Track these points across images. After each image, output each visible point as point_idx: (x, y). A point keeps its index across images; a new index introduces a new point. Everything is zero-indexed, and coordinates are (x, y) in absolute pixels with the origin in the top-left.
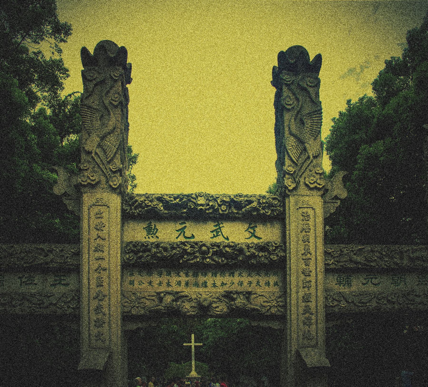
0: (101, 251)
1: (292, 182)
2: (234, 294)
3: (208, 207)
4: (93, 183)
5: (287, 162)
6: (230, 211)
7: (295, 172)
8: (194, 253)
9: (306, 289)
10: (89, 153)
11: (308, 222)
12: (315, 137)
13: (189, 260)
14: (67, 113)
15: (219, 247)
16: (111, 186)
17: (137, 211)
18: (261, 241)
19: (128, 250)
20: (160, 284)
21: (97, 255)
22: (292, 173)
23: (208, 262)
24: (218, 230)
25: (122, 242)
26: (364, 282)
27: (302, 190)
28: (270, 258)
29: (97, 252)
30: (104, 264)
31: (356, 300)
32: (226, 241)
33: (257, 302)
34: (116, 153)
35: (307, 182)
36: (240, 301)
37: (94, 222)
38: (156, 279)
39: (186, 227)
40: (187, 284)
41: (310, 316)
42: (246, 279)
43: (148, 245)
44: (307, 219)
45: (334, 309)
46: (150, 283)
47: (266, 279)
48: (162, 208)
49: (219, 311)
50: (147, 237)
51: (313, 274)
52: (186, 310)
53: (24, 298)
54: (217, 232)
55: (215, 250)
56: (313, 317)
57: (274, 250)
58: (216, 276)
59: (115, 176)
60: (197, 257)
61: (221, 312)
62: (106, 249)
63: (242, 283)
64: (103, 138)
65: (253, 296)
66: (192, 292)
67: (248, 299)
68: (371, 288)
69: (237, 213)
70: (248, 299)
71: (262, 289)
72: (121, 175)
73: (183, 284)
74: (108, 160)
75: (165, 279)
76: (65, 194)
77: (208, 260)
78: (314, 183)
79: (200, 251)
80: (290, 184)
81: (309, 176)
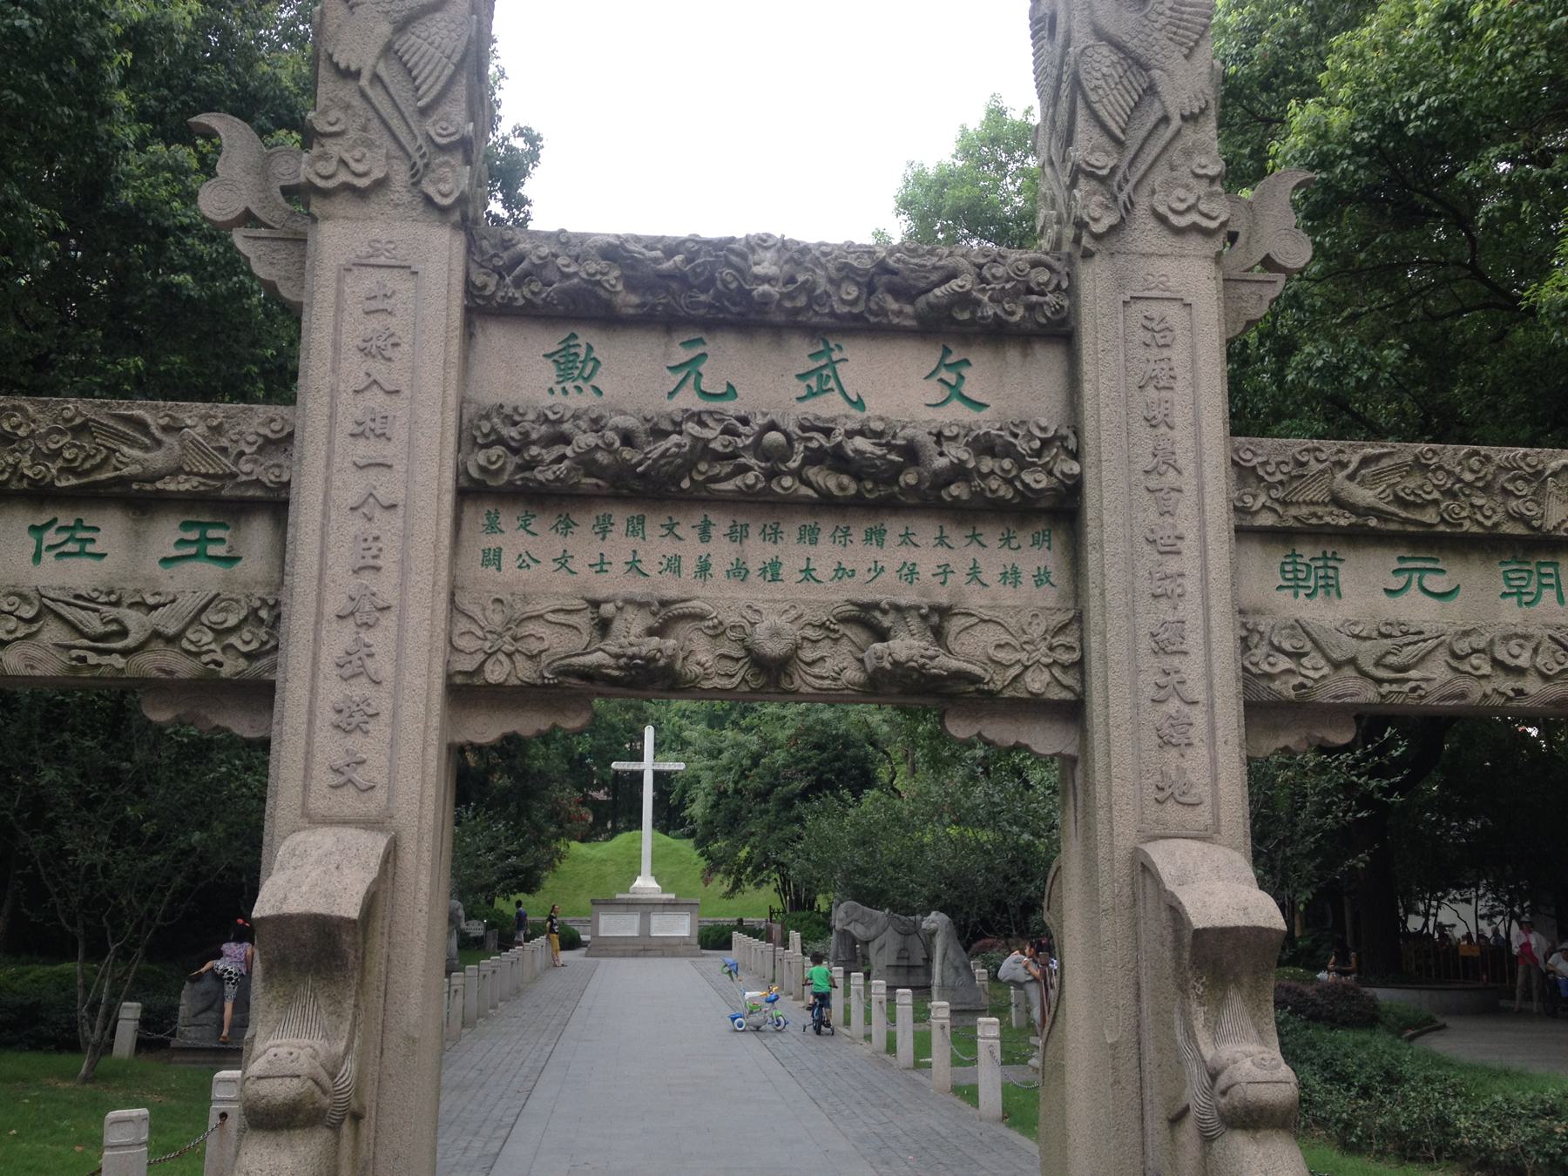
0: (378, 436)
1: (1107, 207)
2: (885, 612)
3: (791, 287)
4: (362, 183)
5: (1085, 131)
6: (873, 306)
7: (1113, 170)
8: (734, 456)
9: (1164, 604)
10: (350, 75)
11: (1166, 353)
12: (1191, 49)
13: (716, 479)
14: (501, 189)
15: (828, 432)
16: (428, 200)
17: (525, 291)
18: (986, 413)
19: (486, 436)
20: (601, 566)
21: (364, 450)
22: (1105, 172)
23: (785, 489)
24: (825, 372)
25: (463, 401)
26: (1396, 583)
27: (1143, 233)
28: (1022, 482)
29: (361, 442)
30: (387, 487)
31: (1367, 653)
32: (854, 412)
33: (969, 651)
34: (451, 81)
35: (1162, 209)
36: (907, 646)
37: (356, 328)
38: (583, 543)
39: (704, 355)
40: (704, 568)
41: (1186, 709)
42: (928, 558)
43: (560, 421)
44: (1162, 342)
45: (1277, 685)
46: (563, 561)
47: (1006, 557)
48: (620, 288)
49: (823, 678)
50: (557, 389)
51: (1189, 547)
52: (698, 670)
53: (45, 612)
54: (820, 380)
55: (814, 445)
56: (1198, 716)
57: (1038, 453)
58: (814, 542)
59: (446, 163)
60: (746, 469)
61: (835, 679)
62: (399, 432)
63: (912, 572)
64: (402, 26)
65: (955, 624)
66: (720, 597)
67: (938, 634)
68: (1417, 610)
69: (900, 313)
70: (938, 634)
71: (990, 598)
72: (468, 161)
73: (689, 566)
74: (420, 104)
75: (619, 545)
76: (247, 218)
77: (787, 481)
78: (1189, 209)
79: (758, 448)
80: (1097, 215)
81: (1170, 185)
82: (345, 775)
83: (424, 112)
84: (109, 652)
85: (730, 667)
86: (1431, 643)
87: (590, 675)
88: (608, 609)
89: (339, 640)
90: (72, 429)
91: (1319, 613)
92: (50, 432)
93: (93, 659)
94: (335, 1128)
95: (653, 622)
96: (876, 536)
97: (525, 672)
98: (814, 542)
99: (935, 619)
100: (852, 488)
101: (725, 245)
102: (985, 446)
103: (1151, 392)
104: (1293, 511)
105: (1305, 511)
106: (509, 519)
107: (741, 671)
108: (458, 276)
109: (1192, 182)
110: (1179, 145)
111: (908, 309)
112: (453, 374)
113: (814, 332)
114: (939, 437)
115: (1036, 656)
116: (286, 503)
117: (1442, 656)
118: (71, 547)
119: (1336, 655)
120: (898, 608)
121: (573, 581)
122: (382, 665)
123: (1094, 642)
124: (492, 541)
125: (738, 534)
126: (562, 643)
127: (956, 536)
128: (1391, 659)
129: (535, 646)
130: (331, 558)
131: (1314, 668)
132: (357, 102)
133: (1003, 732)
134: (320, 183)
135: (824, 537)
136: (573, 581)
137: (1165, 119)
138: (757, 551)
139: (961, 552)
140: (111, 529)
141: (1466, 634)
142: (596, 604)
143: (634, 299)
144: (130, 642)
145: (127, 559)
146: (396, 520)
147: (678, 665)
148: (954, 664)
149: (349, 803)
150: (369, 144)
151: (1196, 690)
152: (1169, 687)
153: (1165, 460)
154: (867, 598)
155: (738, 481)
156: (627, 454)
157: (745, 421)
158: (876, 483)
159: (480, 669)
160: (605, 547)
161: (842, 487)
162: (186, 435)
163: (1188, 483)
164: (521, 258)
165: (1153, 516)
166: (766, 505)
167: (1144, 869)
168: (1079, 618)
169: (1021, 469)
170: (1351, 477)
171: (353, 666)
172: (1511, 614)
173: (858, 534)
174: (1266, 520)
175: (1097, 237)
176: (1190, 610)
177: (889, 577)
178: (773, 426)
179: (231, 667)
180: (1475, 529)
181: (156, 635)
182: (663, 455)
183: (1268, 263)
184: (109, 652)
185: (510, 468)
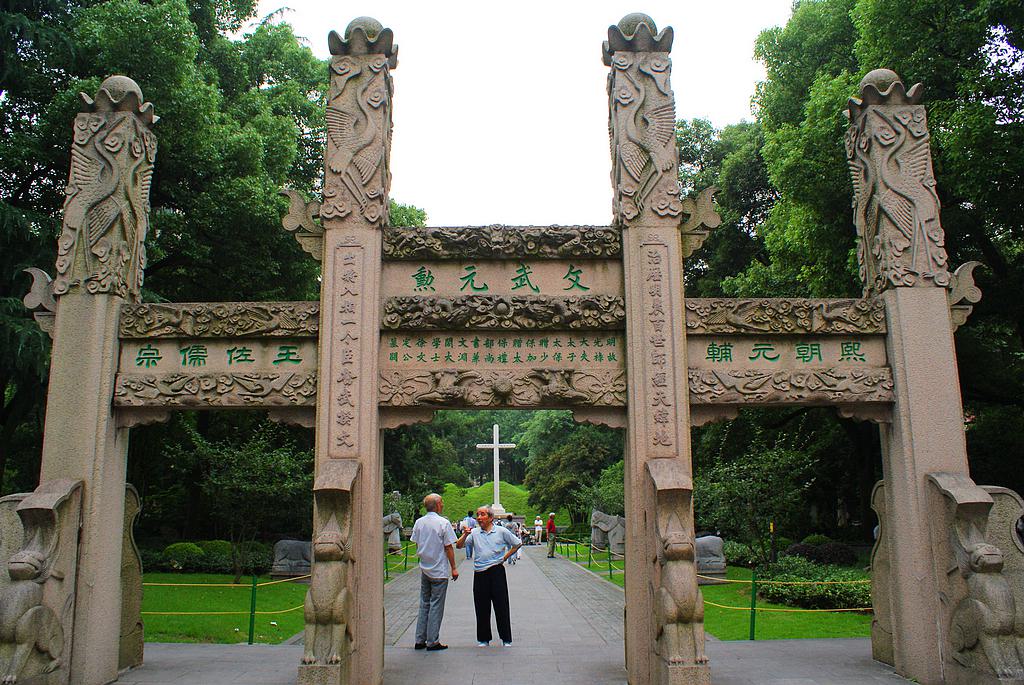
5: (624, 177)
8: (486, 313)
13: (479, 323)
15: (523, 302)
20: (436, 358)
21: (346, 317)
27: (648, 219)
30: (354, 331)
33: (582, 387)
36: (555, 384)
38: (429, 350)
40: (476, 358)
42: (565, 351)
43: (418, 302)
46: (421, 357)
51: (667, 344)
54: (522, 281)
55: (518, 308)
56: (670, 411)
58: (520, 346)
60: (491, 318)
62: (358, 310)
65: (575, 378)
66: (482, 369)
67: (569, 381)
69: (551, 253)
71: (590, 369)
73: (470, 357)
81: (659, 198)
82: (342, 441)
83: (364, 186)
84: (258, 396)
85: (486, 397)
86: (766, 378)
87: (432, 401)
88: (438, 376)
89: (338, 390)
90: (241, 314)
91: (722, 368)
92: (234, 315)
93: (252, 399)
94: (346, 562)
95: (455, 380)
96: (545, 343)
97: (408, 401)
98: (520, 346)
99: (567, 376)
100: (534, 324)
101: (478, 230)
102: (588, 305)
103: (652, 283)
104: (711, 327)
105: (716, 327)
106: (400, 341)
107: (490, 398)
108: (379, 247)
109: (667, 197)
110: (662, 182)
111: (555, 251)
112: (377, 286)
113: (518, 262)
114: (568, 302)
115: (609, 389)
116: (317, 338)
117: (771, 383)
118: (243, 358)
119: (728, 385)
120: (553, 372)
121: (424, 366)
122: (354, 399)
123: (630, 383)
124: (394, 350)
125: (489, 344)
126: (424, 390)
127: (577, 342)
128: (749, 385)
129: (410, 391)
130: (334, 359)
131: (719, 389)
132: (340, 184)
133: (598, 420)
134: (326, 216)
135: (524, 345)
136: (424, 366)
137: (656, 172)
138: (497, 350)
139: (579, 349)
140: (255, 350)
141: (779, 374)
142: (434, 374)
143: (446, 252)
144: (265, 392)
145: (261, 362)
146: (357, 344)
147: (466, 397)
148: (575, 393)
149: (344, 451)
150: (344, 200)
151: (670, 400)
152: (660, 400)
153: (658, 309)
154: (538, 367)
155: (488, 324)
156: (444, 314)
157: (490, 299)
158: (543, 322)
159: (390, 400)
160: (438, 351)
161: (529, 324)
162: (283, 315)
163: (667, 318)
164: (403, 238)
165: (653, 332)
166: (498, 333)
167: (647, 469)
168: (625, 373)
169: (601, 314)
170: (734, 313)
171: (344, 400)
172: (800, 365)
173: (537, 342)
174: (700, 331)
175: (629, 221)
176: (668, 369)
177: (550, 358)
178: (502, 301)
179: (300, 401)
180: (784, 332)
181: (273, 390)
182: (458, 314)
183: (703, 226)
184: (258, 396)
185: (400, 321)
